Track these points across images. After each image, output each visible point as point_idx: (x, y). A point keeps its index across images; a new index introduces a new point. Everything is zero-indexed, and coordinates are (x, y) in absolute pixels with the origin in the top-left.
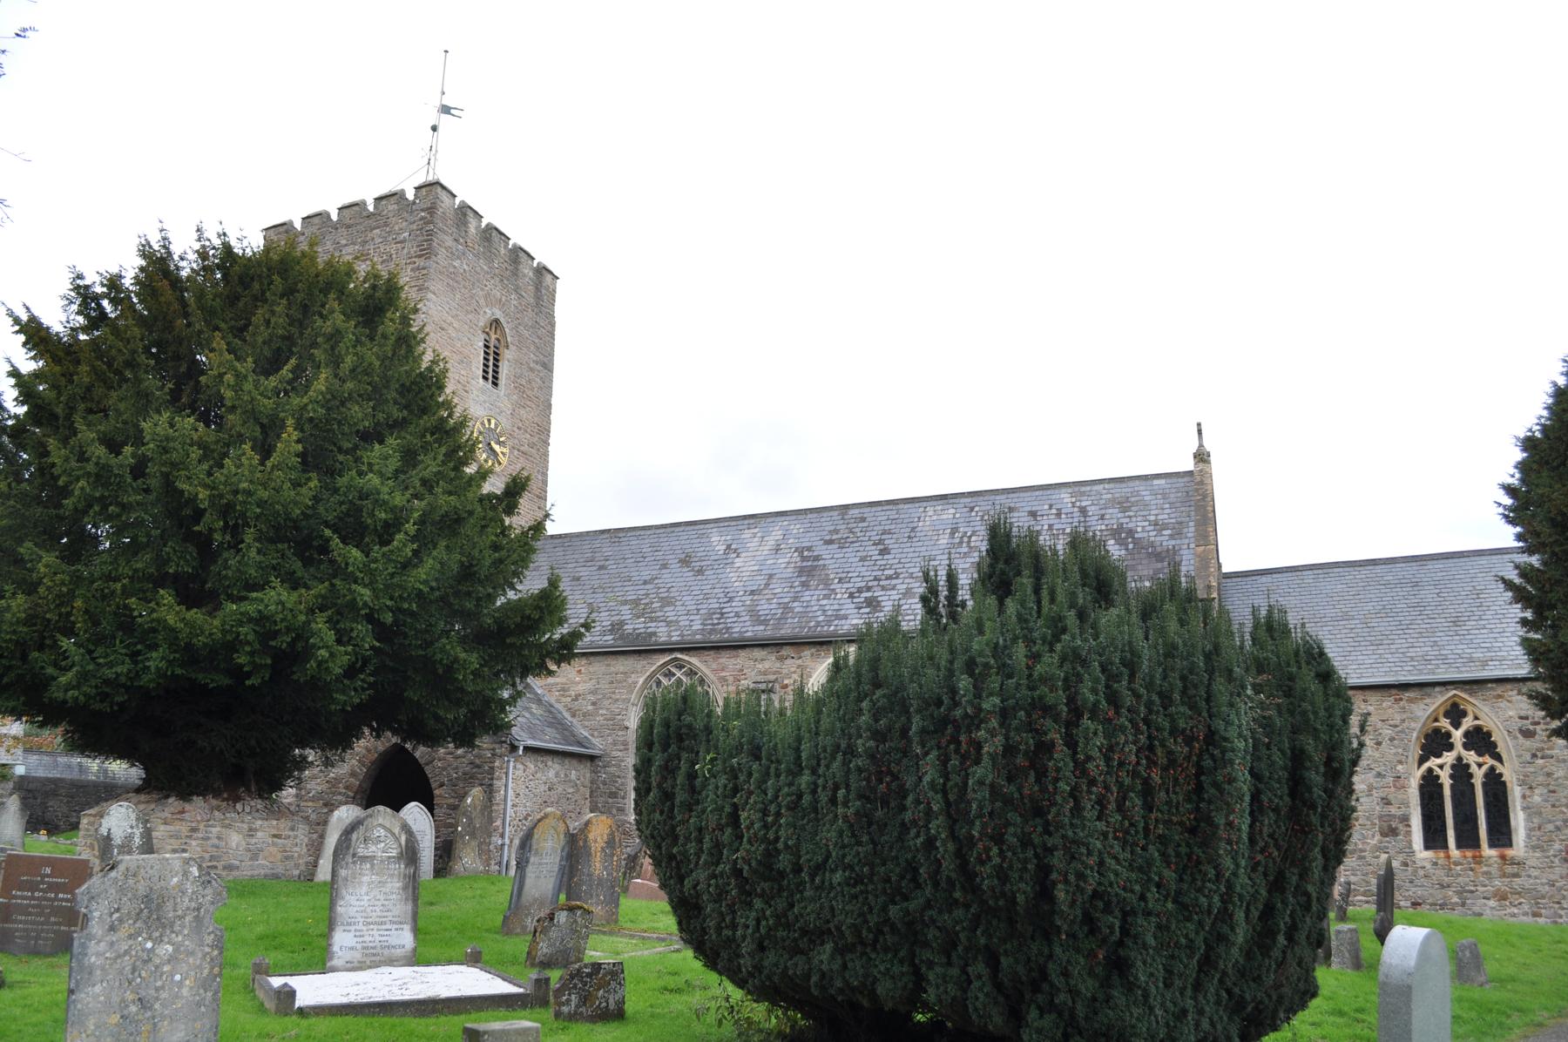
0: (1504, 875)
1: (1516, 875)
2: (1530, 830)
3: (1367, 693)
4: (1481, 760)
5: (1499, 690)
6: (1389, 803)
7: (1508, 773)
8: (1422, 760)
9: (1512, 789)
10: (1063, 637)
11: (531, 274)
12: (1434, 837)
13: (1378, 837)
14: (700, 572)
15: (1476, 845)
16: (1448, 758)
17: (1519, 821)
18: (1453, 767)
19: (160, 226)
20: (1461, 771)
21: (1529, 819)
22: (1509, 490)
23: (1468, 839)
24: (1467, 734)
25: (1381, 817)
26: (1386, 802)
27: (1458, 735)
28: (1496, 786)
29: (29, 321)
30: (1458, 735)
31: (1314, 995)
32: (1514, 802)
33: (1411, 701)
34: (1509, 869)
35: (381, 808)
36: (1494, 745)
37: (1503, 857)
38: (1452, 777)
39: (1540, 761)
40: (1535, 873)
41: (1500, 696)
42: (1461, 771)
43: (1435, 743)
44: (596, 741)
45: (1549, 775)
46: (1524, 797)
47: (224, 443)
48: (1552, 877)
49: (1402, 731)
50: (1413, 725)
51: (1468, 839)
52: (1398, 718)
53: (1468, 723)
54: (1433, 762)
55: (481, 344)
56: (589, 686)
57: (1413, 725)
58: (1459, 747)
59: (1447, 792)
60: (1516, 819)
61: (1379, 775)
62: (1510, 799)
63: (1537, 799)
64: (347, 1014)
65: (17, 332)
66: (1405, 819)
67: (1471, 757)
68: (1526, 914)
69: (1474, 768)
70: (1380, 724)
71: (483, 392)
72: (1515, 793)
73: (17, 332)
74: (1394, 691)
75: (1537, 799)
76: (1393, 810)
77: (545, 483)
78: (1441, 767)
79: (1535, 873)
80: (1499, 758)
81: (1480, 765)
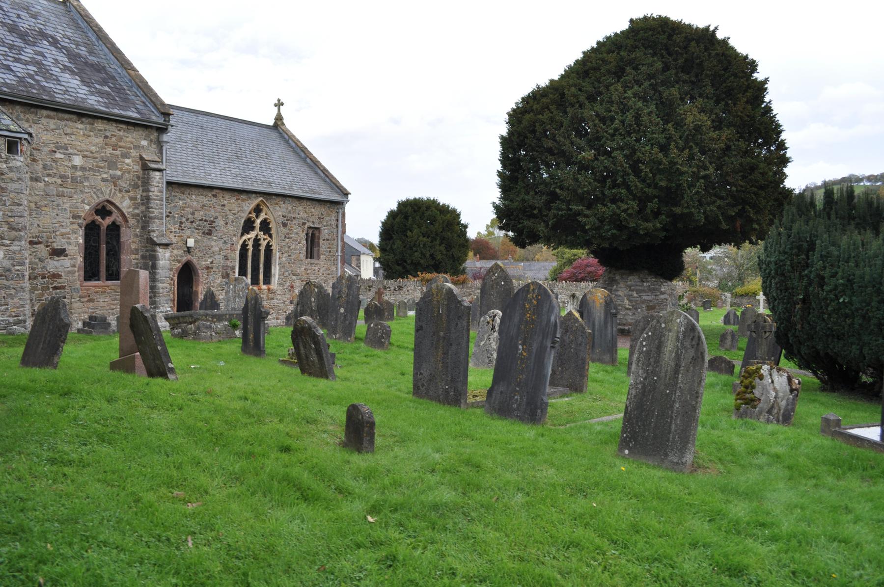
0: (268, 299)
1: (272, 299)
2: (280, 275)
3: (225, 193)
4: (265, 237)
5: (278, 200)
6: (227, 259)
8: (242, 235)
9: (276, 254)
13: (220, 279)
14: (306, 449)
16: (252, 235)
17: (276, 270)
20: (257, 241)
21: (280, 270)
24: (262, 223)
25: (223, 267)
28: (269, 248)
29: (406, 314)
31: (105, 319)
32: (275, 260)
33: (243, 200)
34: (271, 296)
36: (270, 229)
37: (269, 289)
39: (287, 240)
41: (277, 204)
42: (257, 241)
43: (248, 226)
46: (279, 258)
48: (285, 299)
49: (237, 218)
50: (242, 215)
52: (237, 209)
54: (245, 237)
57: (242, 215)
60: (275, 269)
62: (273, 259)
63: (284, 259)
68: (273, 319)
69: (262, 242)
70: (228, 212)
72: (276, 255)
74: (236, 194)
75: (284, 259)
77: (126, 64)
78: (249, 239)
79: (279, 297)
80: (270, 236)
81: (264, 240)
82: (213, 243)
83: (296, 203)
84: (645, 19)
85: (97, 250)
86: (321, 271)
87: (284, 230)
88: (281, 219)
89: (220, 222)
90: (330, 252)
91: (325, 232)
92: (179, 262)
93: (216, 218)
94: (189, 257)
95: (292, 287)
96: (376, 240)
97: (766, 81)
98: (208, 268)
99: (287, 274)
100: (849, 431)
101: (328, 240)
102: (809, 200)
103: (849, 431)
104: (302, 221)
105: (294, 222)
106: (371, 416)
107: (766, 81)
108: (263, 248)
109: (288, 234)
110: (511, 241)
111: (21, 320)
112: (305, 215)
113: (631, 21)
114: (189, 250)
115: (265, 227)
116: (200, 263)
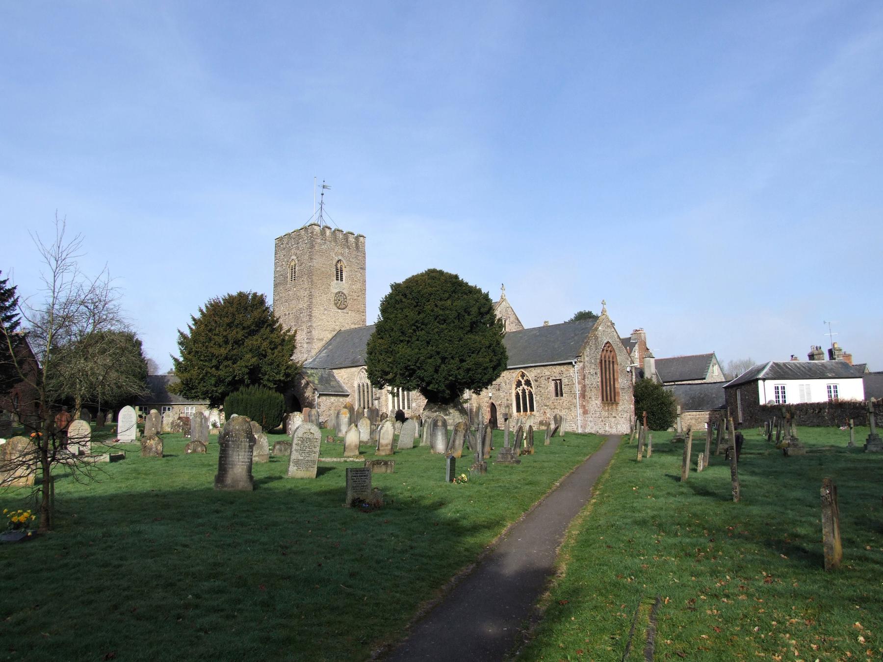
7: (533, 391)
10: (467, 394)
11: (354, 240)
12: (518, 410)
16: (521, 388)
20: (524, 391)
22: (476, 287)
23: (525, 410)
26: (507, 400)
27: (523, 382)
28: (531, 394)
30: (523, 382)
33: (513, 373)
36: (531, 384)
43: (519, 384)
44: (349, 391)
51: (525, 410)
58: (523, 385)
63: (538, 398)
64: (302, 479)
65: (201, 311)
66: (511, 404)
67: (526, 387)
71: (337, 284)
73: (201, 311)
75: (538, 398)
80: (531, 387)
83: (543, 368)
84: (407, 280)
86: (565, 403)
88: (534, 378)
91: (565, 381)
94: (491, 401)
96: (787, 403)
102: (165, 381)
106: (476, 537)
108: (527, 394)
111: (695, 576)
112: (549, 373)
113: (392, 286)
114: (490, 398)
115: (528, 383)
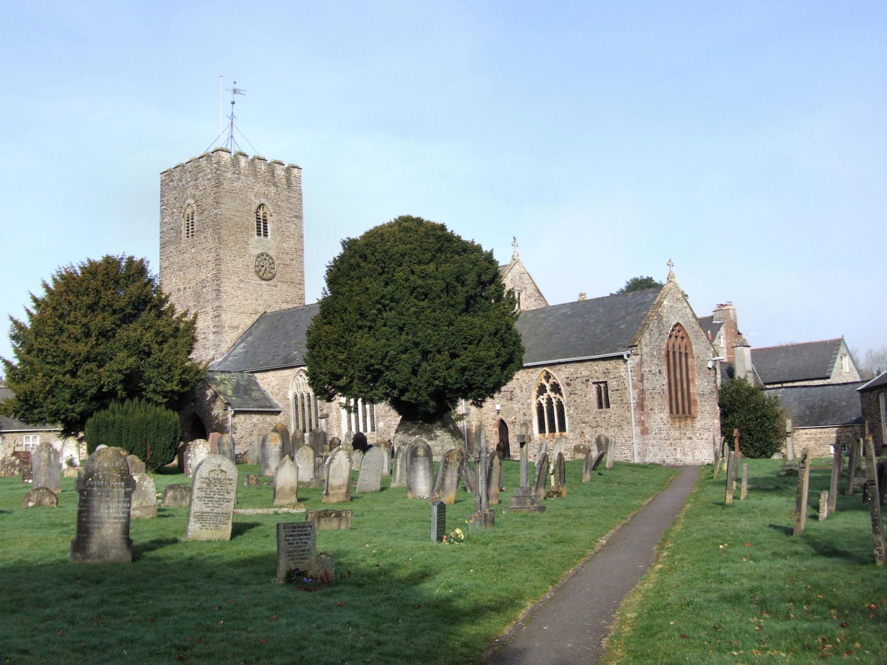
5: (559, 367)
7: (564, 400)
12: (542, 429)
15: (555, 431)
16: (545, 396)
18: (547, 399)
19: (233, 86)
20: (549, 401)
21: (569, 419)
23: (552, 430)
26: (525, 415)
33: (532, 373)
35: (198, 441)
36: (560, 390)
38: (546, 403)
40: (571, 441)
42: (549, 401)
43: (542, 390)
45: (575, 401)
47: (401, 255)
51: (552, 430)
52: (527, 380)
53: (551, 381)
55: (254, 219)
56: (276, 382)
58: (549, 391)
59: (545, 410)
61: (522, 404)
63: (571, 411)
66: (531, 421)
67: (552, 395)
71: (258, 242)
75: (572, 411)
76: (527, 417)
80: (561, 395)
82: (514, 406)
83: (578, 365)
85: (549, 419)
86: (613, 418)
87: (569, 389)
88: (566, 381)
89: (518, 391)
90: (622, 400)
91: (612, 384)
92: (494, 420)
93: (514, 388)
95: (583, 433)
97: (452, 231)
98: (513, 422)
99: (576, 423)
100: (167, 466)
101: (618, 390)
103: (167, 466)
104: (584, 379)
105: (577, 380)
107: (452, 231)
109: (573, 391)
110: (167, 408)
114: (498, 412)
115: (556, 388)
116: (508, 421)
